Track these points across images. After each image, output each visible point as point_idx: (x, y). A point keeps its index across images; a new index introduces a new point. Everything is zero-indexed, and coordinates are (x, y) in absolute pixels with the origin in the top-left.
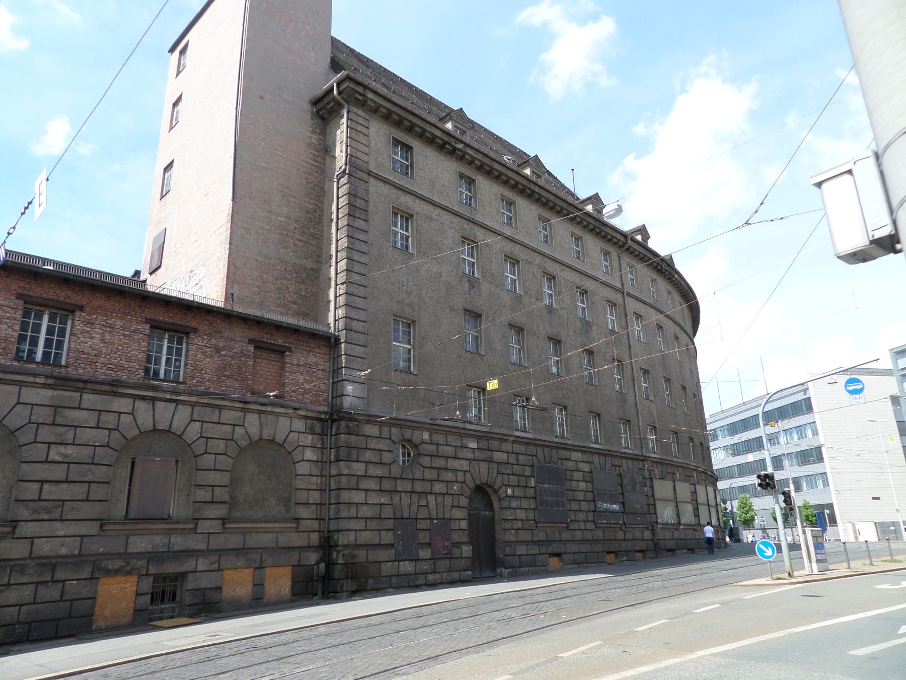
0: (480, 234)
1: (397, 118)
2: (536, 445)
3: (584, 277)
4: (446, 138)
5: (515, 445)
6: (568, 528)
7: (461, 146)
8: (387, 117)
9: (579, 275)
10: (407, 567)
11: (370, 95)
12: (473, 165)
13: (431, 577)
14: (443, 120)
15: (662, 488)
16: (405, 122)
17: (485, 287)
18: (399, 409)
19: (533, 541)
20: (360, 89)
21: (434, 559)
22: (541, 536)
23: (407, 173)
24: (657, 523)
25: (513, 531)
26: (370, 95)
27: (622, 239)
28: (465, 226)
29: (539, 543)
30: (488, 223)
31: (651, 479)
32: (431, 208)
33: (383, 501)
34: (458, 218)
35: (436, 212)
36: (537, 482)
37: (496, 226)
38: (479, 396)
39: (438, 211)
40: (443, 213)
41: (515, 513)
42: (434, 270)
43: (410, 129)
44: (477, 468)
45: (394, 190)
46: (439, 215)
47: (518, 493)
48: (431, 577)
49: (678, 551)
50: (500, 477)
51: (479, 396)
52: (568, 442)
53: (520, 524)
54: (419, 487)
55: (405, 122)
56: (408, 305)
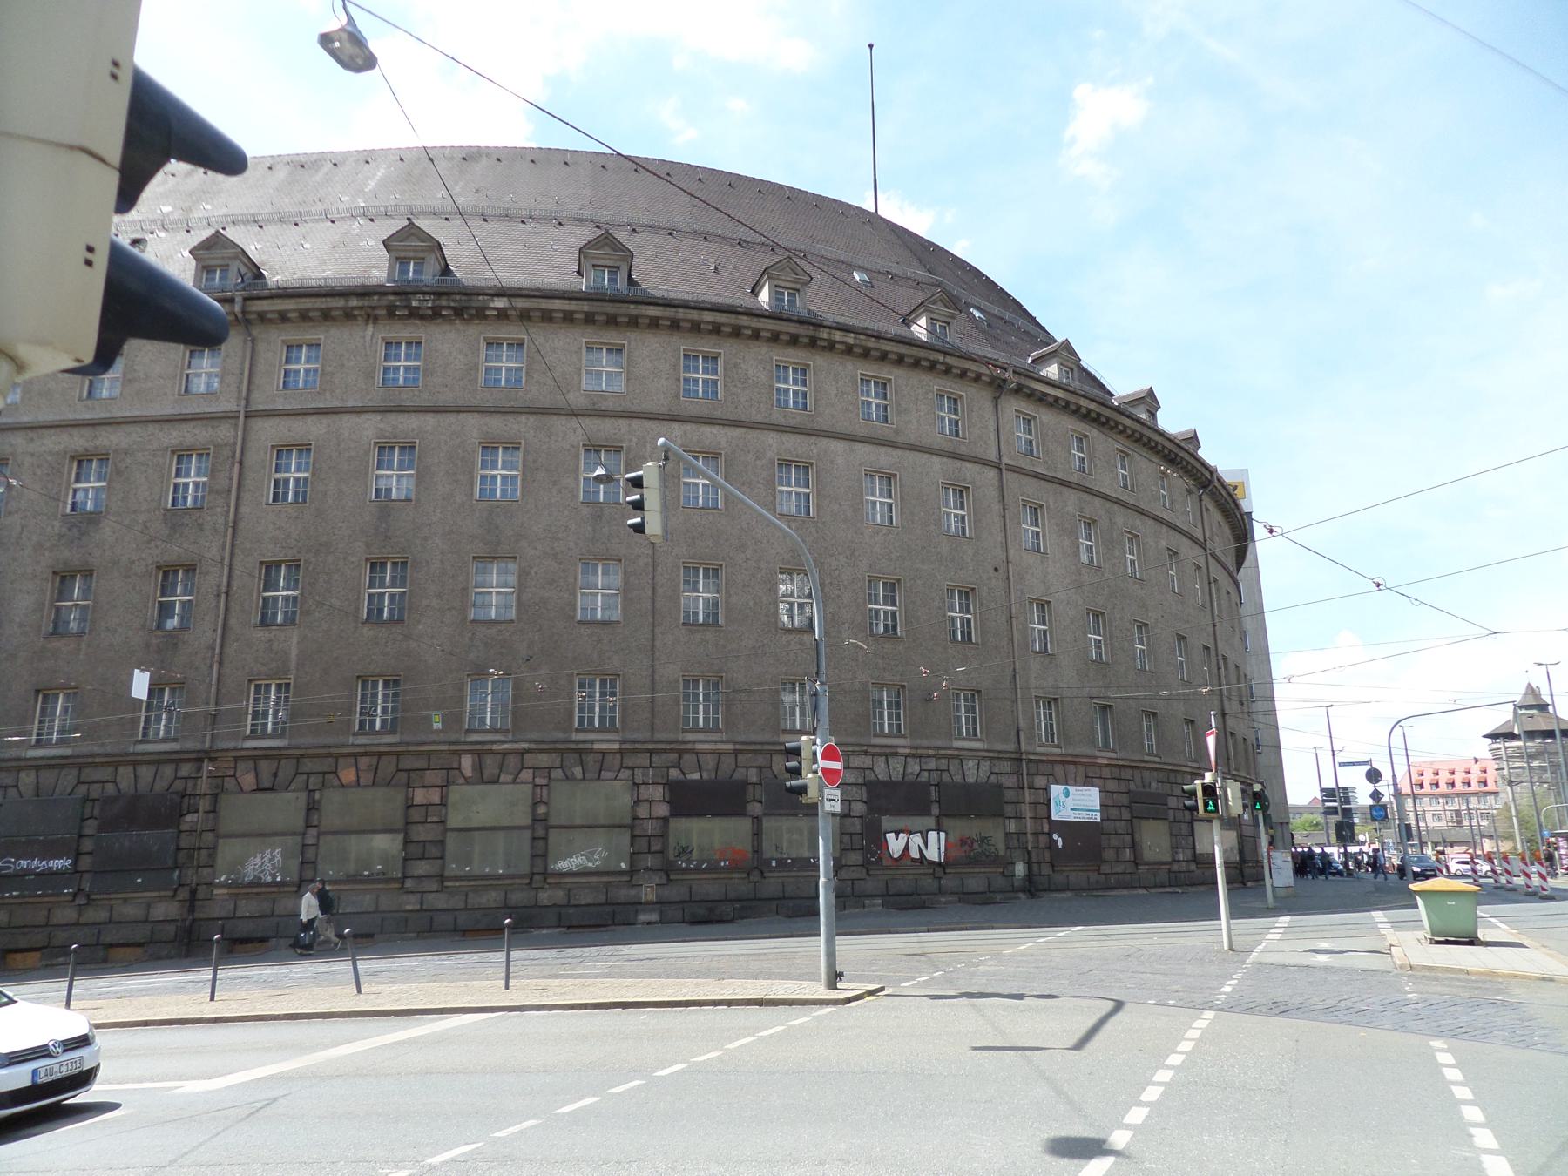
0: (109, 439)
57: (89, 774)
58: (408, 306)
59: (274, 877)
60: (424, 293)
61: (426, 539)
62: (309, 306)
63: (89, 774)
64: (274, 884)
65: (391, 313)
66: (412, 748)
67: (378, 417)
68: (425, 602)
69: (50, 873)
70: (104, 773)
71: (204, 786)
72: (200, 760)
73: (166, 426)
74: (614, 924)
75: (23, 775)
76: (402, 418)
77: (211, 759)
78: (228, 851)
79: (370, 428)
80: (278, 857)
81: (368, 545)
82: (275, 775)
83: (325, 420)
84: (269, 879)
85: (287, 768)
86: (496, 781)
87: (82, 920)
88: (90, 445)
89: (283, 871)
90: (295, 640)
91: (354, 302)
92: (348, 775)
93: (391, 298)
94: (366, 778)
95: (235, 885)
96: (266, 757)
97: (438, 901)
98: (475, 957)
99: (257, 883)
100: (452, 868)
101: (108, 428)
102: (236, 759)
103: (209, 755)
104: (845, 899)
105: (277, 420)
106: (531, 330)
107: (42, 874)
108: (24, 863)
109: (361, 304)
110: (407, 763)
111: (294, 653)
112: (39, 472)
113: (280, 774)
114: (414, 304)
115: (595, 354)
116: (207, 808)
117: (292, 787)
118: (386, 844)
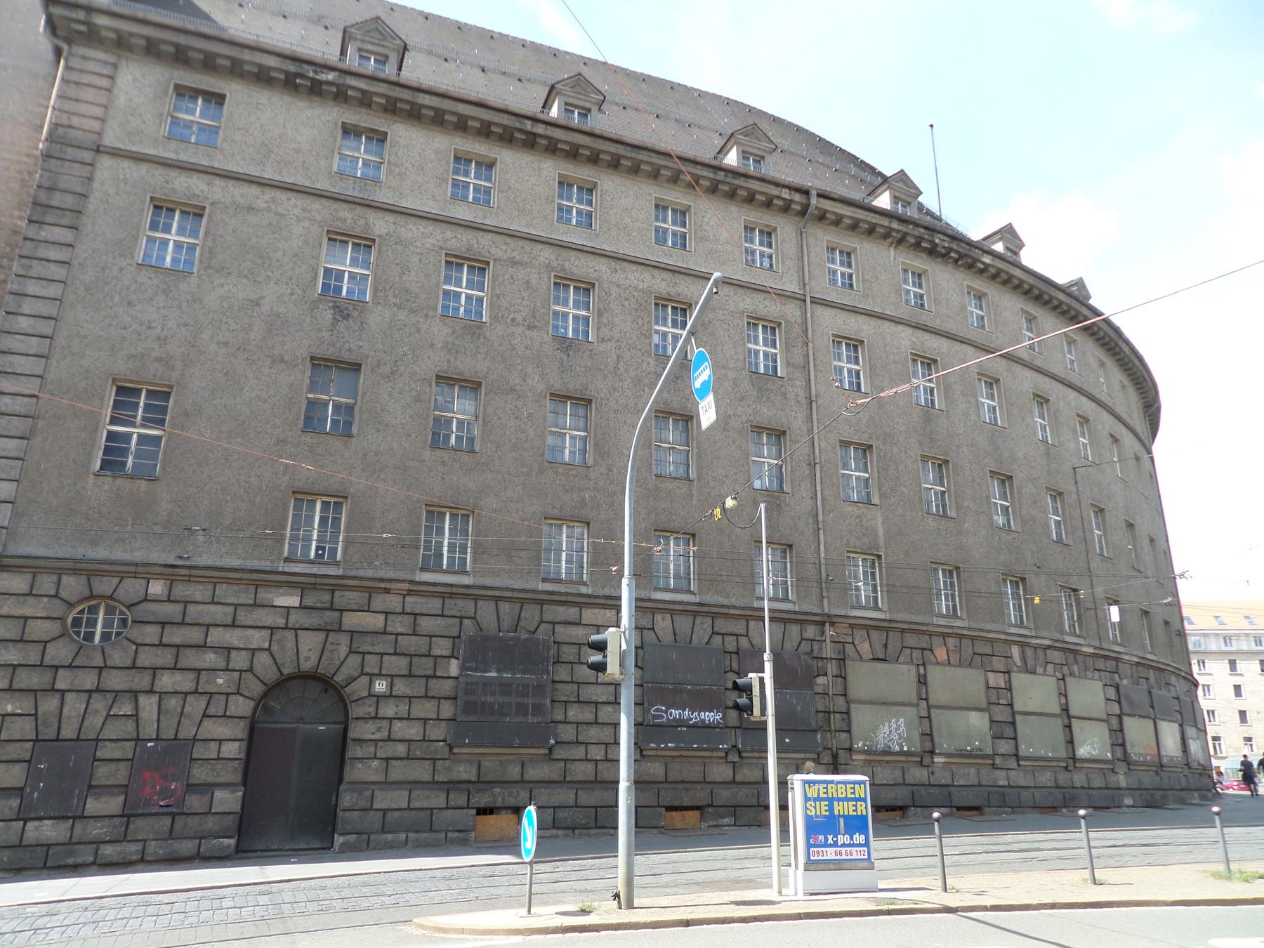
0: (380, 225)
1: (383, 101)
2: (476, 598)
3: (679, 278)
4: (292, 68)
5: (409, 599)
6: (549, 757)
7: (331, 76)
8: (151, 50)
9: (666, 275)
10: (47, 831)
11: (101, 20)
12: (842, 225)
13: (108, 851)
14: (873, 193)
15: (866, 679)
16: (757, 196)
17: (377, 318)
18: (94, 543)
19: (434, 782)
20: (81, 15)
21: (127, 815)
22: (464, 772)
23: (851, 285)
24: (850, 749)
25: (375, 763)
26: (101, 20)
27: (797, 197)
28: (449, 234)
29: (450, 786)
30: (409, 203)
31: (842, 661)
32: (254, 190)
33: (9, 708)
34: (325, 202)
35: (267, 197)
36: (463, 668)
37: (432, 208)
38: (873, 567)
39: (269, 194)
40: (279, 194)
41: (395, 727)
42: (241, 295)
43: (209, 64)
44: (290, 645)
45: (161, 170)
46: (274, 200)
47: (401, 687)
48: (108, 851)
49: (987, 810)
50: (354, 661)
51: (873, 567)
52: (584, 590)
53: (401, 749)
54: (115, 681)
55: (375, 99)
56: (158, 360)
57: (721, 625)
58: (932, 242)
59: (902, 747)
60: (945, 234)
61: (958, 447)
62: (862, 217)
63: (721, 625)
64: (901, 753)
65: (917, 246)
66: (982, 634)
67: (910, 331)
68: (966, 504)
69: (704, 726)
70: (739, 627)
71: (829, 650)
72: (823, 623)
73: (740, 291)
74: (45, 867)
75: (658, 617)
76: (927, 336)
77: (832, 624)
78: (862, 717)
79: (906, 339)
80: (903, 728)
81: (921, 444)
82: (886, 646)
83: (873, 322)
84: (897, 748)
85: (894, 639)
86: (1034, 672)
87: (738, 778)
88: (673, 291)
89: (908, 740)
90: (880, 520)
91: (895, 225)
92: (941, 654)
93: (922, 230)
94: (954, 658)
95: (868, 752)
96: (876, 628)
97: (1019, 778)
98: (743, 852)
99: (887, 752)
100: (1024, 750)
101: (414, 219)
102: (852, 626)
103: (824, 621)
104: (641, 823)
105: (834, 311)
106: (865, 244)
107: (694, 726)
108: (675, 713)
109: (900, 228)
110: (980, 648)
111: (881, 532)
112: (626, 304)
113: (890, 646)
114: (937, 241)
115: (351, 142)
116: (835, 673)
117: (901, 659)
118: (978, 721)
